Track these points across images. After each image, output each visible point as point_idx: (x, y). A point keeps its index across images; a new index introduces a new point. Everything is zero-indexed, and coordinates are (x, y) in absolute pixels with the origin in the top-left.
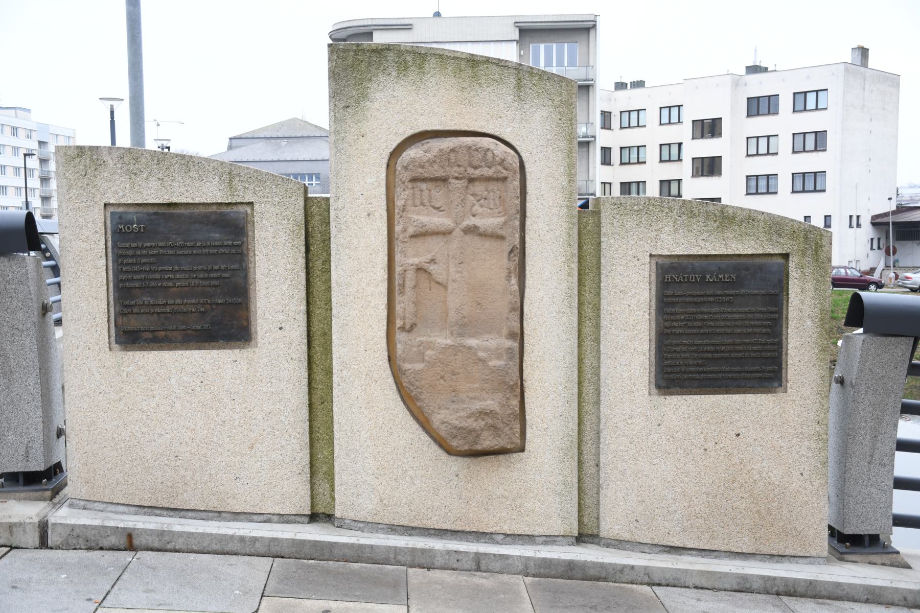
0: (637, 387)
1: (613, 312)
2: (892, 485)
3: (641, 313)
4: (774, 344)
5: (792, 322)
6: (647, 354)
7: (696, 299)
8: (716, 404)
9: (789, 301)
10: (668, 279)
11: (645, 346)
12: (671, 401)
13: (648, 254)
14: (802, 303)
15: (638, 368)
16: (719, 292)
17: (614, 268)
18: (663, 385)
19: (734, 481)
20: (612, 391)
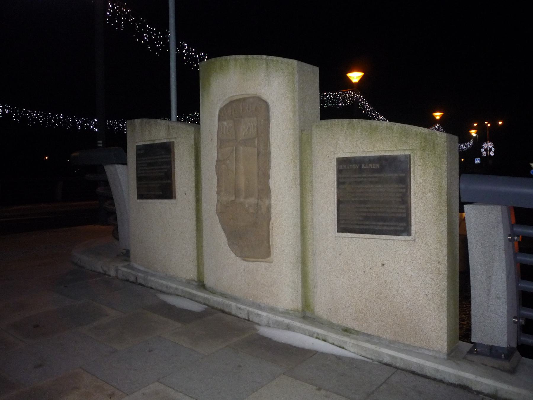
14: (425, 181)
15: (330, 220)
16: (370, 176)
19: (381, 294)
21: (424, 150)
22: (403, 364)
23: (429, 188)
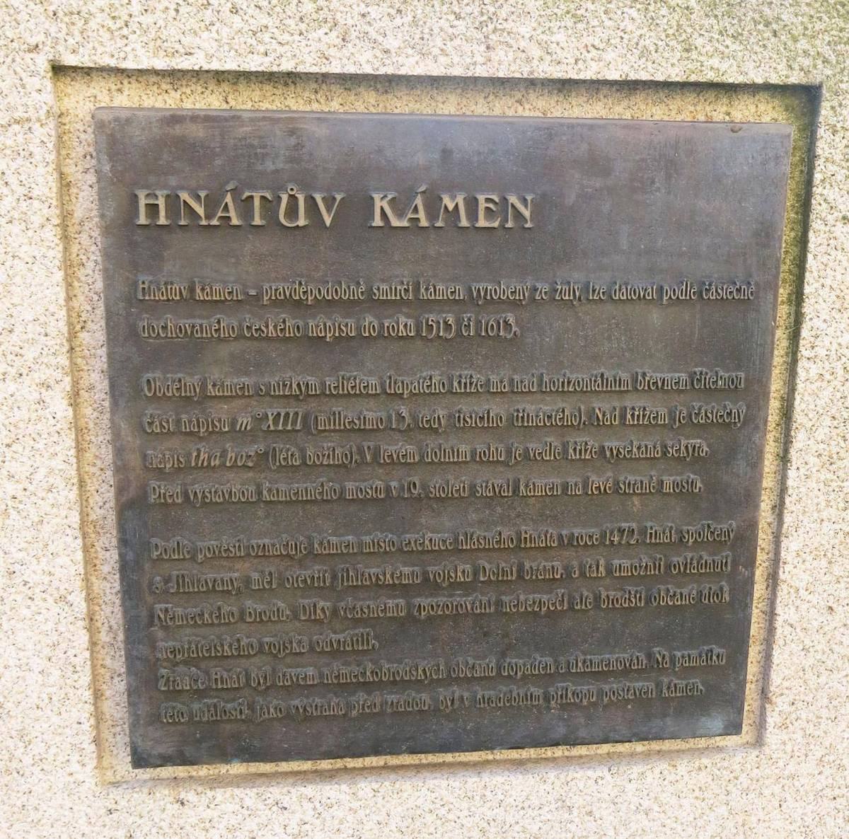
0: (37, 748)
2: (825, 92)
3: (27, 390)
4: (717, 545)
5: (811, 430)
6: (79, 599)
7: (317, 325)
8: (430, 818)
9: (805, 333)
10: (152, 209)
11: (63, 560)
12: (209, 814)
13: (42, 62)
15: (38, 663)
18: (161, 750)
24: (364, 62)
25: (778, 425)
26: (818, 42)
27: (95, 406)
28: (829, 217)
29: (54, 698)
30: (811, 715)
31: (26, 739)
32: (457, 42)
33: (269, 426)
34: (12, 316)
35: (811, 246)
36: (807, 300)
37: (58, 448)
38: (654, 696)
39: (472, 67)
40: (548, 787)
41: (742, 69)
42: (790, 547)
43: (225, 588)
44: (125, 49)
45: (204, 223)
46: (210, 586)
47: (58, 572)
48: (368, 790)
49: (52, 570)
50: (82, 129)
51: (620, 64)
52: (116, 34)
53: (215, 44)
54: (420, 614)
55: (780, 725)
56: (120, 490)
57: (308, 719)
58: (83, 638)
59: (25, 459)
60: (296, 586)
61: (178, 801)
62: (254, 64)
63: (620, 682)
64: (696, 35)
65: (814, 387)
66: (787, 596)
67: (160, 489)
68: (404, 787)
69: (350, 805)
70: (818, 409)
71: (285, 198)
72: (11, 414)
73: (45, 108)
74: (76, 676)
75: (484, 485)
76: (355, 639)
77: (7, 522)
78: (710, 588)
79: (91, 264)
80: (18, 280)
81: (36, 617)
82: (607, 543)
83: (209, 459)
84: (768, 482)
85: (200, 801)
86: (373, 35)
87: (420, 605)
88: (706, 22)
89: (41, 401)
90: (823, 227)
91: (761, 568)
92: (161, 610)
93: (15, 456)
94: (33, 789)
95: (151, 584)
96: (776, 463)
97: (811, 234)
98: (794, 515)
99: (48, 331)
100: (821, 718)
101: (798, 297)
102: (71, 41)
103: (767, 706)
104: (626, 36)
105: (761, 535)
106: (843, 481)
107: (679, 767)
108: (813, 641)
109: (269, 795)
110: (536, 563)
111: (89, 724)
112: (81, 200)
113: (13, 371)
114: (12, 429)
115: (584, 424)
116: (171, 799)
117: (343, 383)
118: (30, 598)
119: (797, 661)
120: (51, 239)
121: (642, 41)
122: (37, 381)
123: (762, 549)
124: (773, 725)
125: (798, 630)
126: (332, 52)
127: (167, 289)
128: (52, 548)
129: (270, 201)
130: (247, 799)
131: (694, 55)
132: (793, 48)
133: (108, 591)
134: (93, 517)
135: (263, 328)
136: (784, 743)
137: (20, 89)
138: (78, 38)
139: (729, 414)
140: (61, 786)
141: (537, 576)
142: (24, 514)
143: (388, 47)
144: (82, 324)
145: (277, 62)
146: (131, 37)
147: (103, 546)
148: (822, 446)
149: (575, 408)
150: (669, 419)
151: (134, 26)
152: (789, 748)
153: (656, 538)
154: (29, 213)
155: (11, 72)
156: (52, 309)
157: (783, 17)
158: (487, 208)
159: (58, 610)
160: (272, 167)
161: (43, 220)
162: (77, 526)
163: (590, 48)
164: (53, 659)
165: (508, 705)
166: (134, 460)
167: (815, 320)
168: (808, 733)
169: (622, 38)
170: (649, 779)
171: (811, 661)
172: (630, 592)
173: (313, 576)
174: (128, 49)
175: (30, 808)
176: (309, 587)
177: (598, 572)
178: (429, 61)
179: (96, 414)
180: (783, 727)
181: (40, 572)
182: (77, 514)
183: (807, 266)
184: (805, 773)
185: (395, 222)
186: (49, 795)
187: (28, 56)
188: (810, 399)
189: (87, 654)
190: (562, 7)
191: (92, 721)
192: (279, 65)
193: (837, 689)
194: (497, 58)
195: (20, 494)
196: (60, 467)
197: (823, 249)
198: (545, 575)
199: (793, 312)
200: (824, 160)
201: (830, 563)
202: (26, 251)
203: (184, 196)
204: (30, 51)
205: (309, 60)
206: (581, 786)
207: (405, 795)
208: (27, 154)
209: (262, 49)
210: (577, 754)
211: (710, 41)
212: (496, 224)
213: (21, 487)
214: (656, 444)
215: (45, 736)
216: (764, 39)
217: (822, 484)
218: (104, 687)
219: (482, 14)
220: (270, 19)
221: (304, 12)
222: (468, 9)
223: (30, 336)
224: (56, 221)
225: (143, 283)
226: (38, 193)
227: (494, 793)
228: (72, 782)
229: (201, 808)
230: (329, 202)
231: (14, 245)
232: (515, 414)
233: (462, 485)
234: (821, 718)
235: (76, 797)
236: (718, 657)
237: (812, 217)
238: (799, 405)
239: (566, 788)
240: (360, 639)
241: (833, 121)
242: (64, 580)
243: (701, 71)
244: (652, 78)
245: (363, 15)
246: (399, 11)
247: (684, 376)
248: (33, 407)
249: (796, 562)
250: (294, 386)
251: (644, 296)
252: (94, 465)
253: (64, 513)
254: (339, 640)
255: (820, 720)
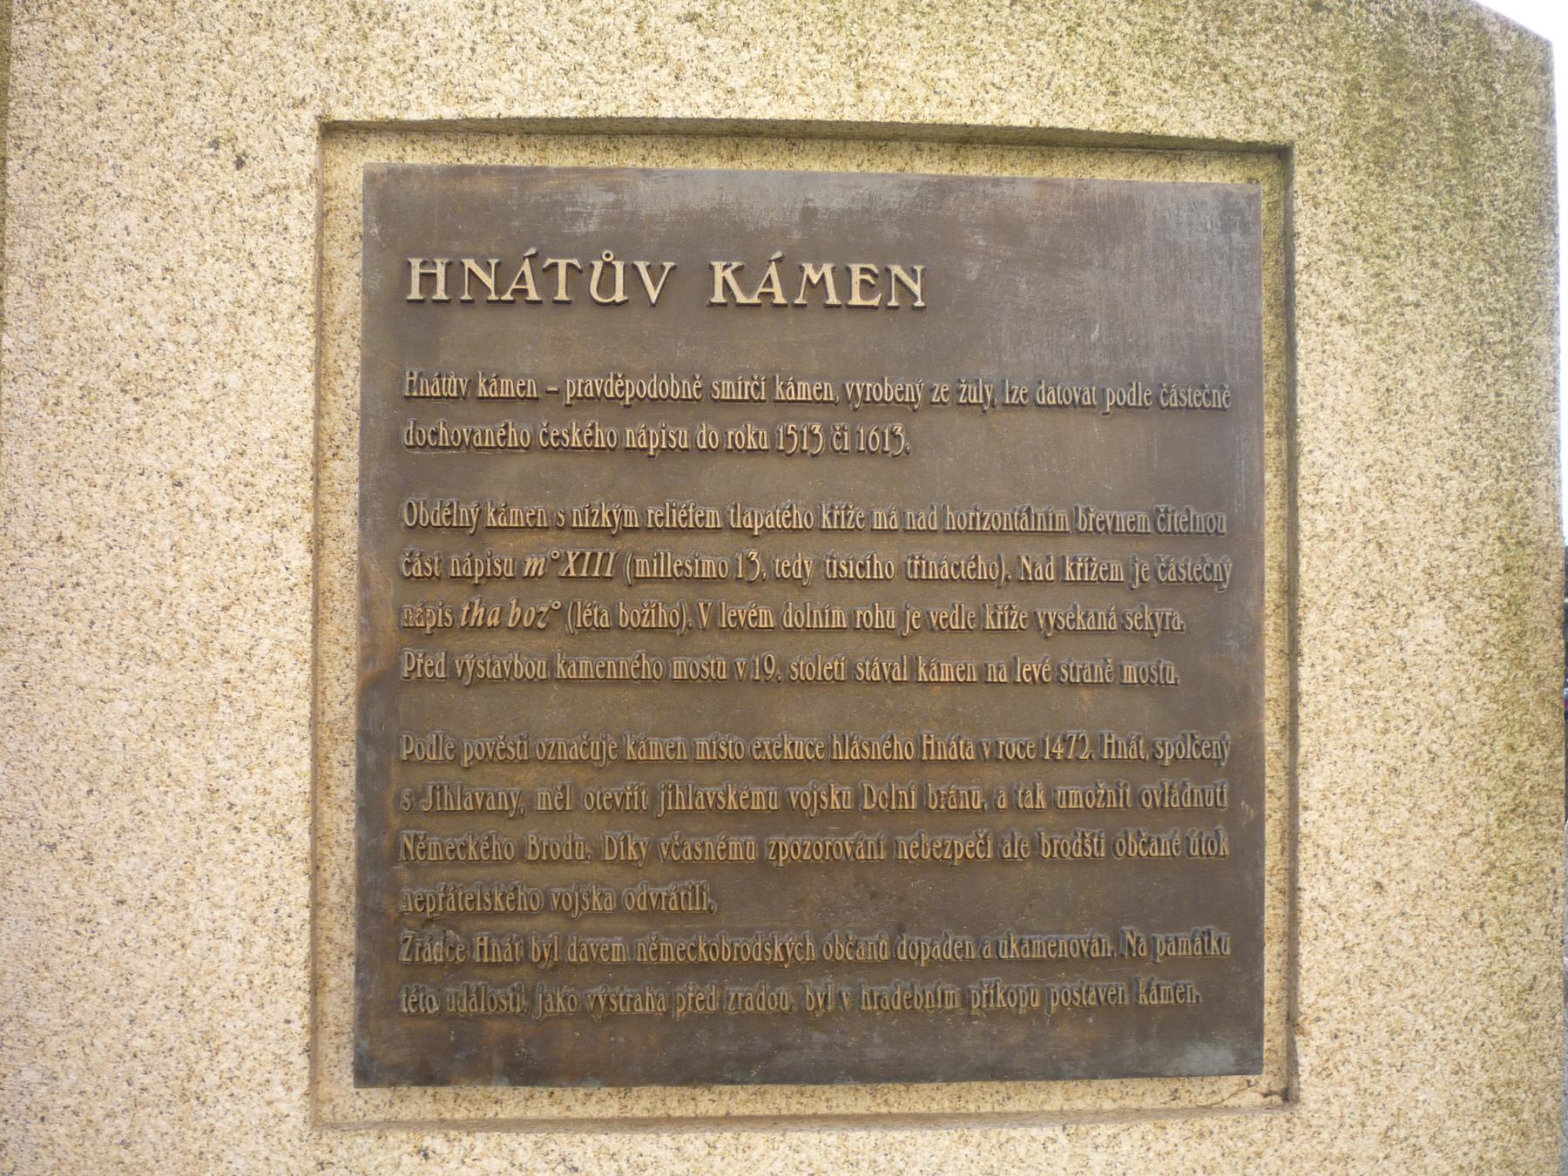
0: (227, 1061)
1: (69, 530)
3: (256, 534)
5: (1326, 610)
6: (300, 831)
7: (640, 435)
9: (1303, 469)
10: (428, 279)
13: (308, 118)
14: (1389, 483)
15: (236, 928)
17: (84, 222)
20: (65, 1085)
21: (1384, 166)
22: (1120, 250)
23: (1420, 553)
24: (700, 104)
25: (1278, 607)
26: (1282, 91)
27: (344, 559)
28: (1321, 314)
29: (257, 982)
30: (1365, 1057)
31: (213, 1045)
32: (821, 79)
33: (568, 571)
34: (245, 434)
35: (1301, 352)
36: (1302, 425)
37: (289, 611)
38: (1126, 1002)
39: (839, 110)
40: (970, 1151)
41: (1187, 120)
42: (1312, 784)
43: (500, 808)
44: (408, 97)
45: (493, 297)
46: (479, 803)
47: (275, 789)
48: (699, 1143)
49: (269, 787)
50: (351, 205)
51: (1028, 107)
52: (399, 80)
53: (517, 87)
54: (778, 858)
55: (1319, 1069)
56: (366, 659)
57: (611, 1018)
58: (301, 889)
59: (244, 627)
60: (599, 808)
61: (419, 1152)
62: (567, 108)
63: (1074, 980)
64: (1123, 75)
65: (1324, 547)
66: (1314, 861)
67: (414, 659)
68: (753, 1142)
69: (672, 1168)
70: (1332, 579)
71: (598, 265)
72: (231, 565)
73: (307, 172)
74: (288, 948)
75: (868, 664)
76: (682, 894)
77: (215, 717)
78: (1201, 834)
79: (351, 373)
80: (256, 386)
81: (242, 856)
82: (1047, 757)
83: (485, 617)
84: (1272, 689)
85: (451, 1152)
86: (713, 71)
87: (777, 845)
88: (1137, 62)
89: (271, 547)
90: (1313, 327)
91: (1270, 821)
92: (409, 838)
93: (234, 622)
94: (217, 1125)
95: (398, 798)
96: (1280, 662)
97: (1299, 336)
98: (1313, 735)
99: (289, 452)
100: (1380, 1063)
101: (1290, 424)
102: (344, 91)
103: (1297, 1038)
104: (1034, 74)
105: (1269, 771)
106: (1378, 690)
107: (1170, 1131)
108: (1357, 936)
109: (553, 1146)
110: (945, 786)
111: (301, 1024)
112: (344, 291)
113: (240, 507)
114: (232, 585)
115: (1006, 579)
116: (410, 1148)
117: (671, 513)
118: (236, 828)
119: (1337, 967)
120: (301, 332)
121: (1055, 79)
122: (270, 519)
123: (1271, 792)
124: (1309, 1068)
125: (1334, 916)
126: (662, 92)
127: (441, 382)
128: (271, 754)
129: (580, 271)
130: (520, 1152)
131: (1123, 99)
132: (1250, 97)
133: (344, 825)
134: (330, 716)
135: (565, 436)
136: (1328, 1102)
137: (279, 151)
138: (353, 86)
139: (1210, 570)
140: (255, 1122)
141: (946, 806)
142: (238, 705)
143: (733, 85)
144: (334, 450)
145: (594, 106)
146: (415, 83)
147: (340, 758)
148: (1344, 635)
149: (992, 558)
150: (1125, 576)
151: (421, 69)
152: (1335, 1110)
153: (1117, 753)
154: (277, 301)
155: (271, 131)
156: (296, 422)
157: (1234, 59)
158: (863, 281)
159: (272, 847)
160: (584, 230)
161: (294, 309)
162: (304, 721)
163: (989, 87)
164: (260, 922)
165: (908, 1008)
166: (387, 620)
167: (1317, 453)
168: (1362, 1086)
169: (1029, 76)
170: (1125, 1148)
171: (1358, 968)
172: (1083, 836)
173: (624, 795)
174: (412, 97)
175: (210, 1156)
176: (614, 811)
177: (1035, 803)
178: (785, 103)
179: (343, 571)
180: (1324, 1074)
181: (251, 789)
182: (307, 704)
183: (1299, 378)
184: (1364, 1155)
185: (741, 298)
186: (237, 1135)
187: (291, 113)
188: (1320, 564)
189: (306, 914)
190: (950, 38)
191: (306, 1019)
192: (596, 110)
193: (1401, 1018)
194: (870, 99)
195: (234, 676)
196: (290, 638)
197: (1316, 356)
198: (958, 804)
199: (1284, 447)
200: (1306, 239)
201: (1372, 813)
202: (270, 348)
203: (470, 263)
204: (294, 106)
205: (633, 101)
206: (1022, 1152)
207: (755, 1155)
208: (281, 228)
209: (575, 91)
210: (1014, 1110)
211: (1143, 83)
212: (875, 302)
213: (235, 666)
214: (1109, 611)
215: (239, 1043)
216: (1212, 84)
217: (1349, 692)
218: (328, 971)
219: (850, 46)
220: (586, 56)
221: (629, 46)
222: (833, 41)
223: (266, 458)
224: (310, 310)
225: (411, 375)
226: (290, 274)
227: (889, 1157)
228: (271, 1114)
229: (453, 1165)
230: (655, 273)
231: (255, 341)
232: (909, 562)
233: (836, 663)
234: (1380, 1063)
235: (274, 1141)
236: (1219, 942)
237: (1298, 313)
238: (1307, 572)
239: (1000, 1154)
240: (690, 894)
241: (1312, 190)
242: (282, 802)
243: (1135, 119)
244: (1071, 126)
245: (702, 49)
246: (746, 44)
247: (1142, 515)
248: (261, 554)
249: (1321, 807)
250: (605, 515)
251: (1080, 400)
252: (337, 642)
253: (289, 703)
254: (660, 895)
255: (1379, 1067)
